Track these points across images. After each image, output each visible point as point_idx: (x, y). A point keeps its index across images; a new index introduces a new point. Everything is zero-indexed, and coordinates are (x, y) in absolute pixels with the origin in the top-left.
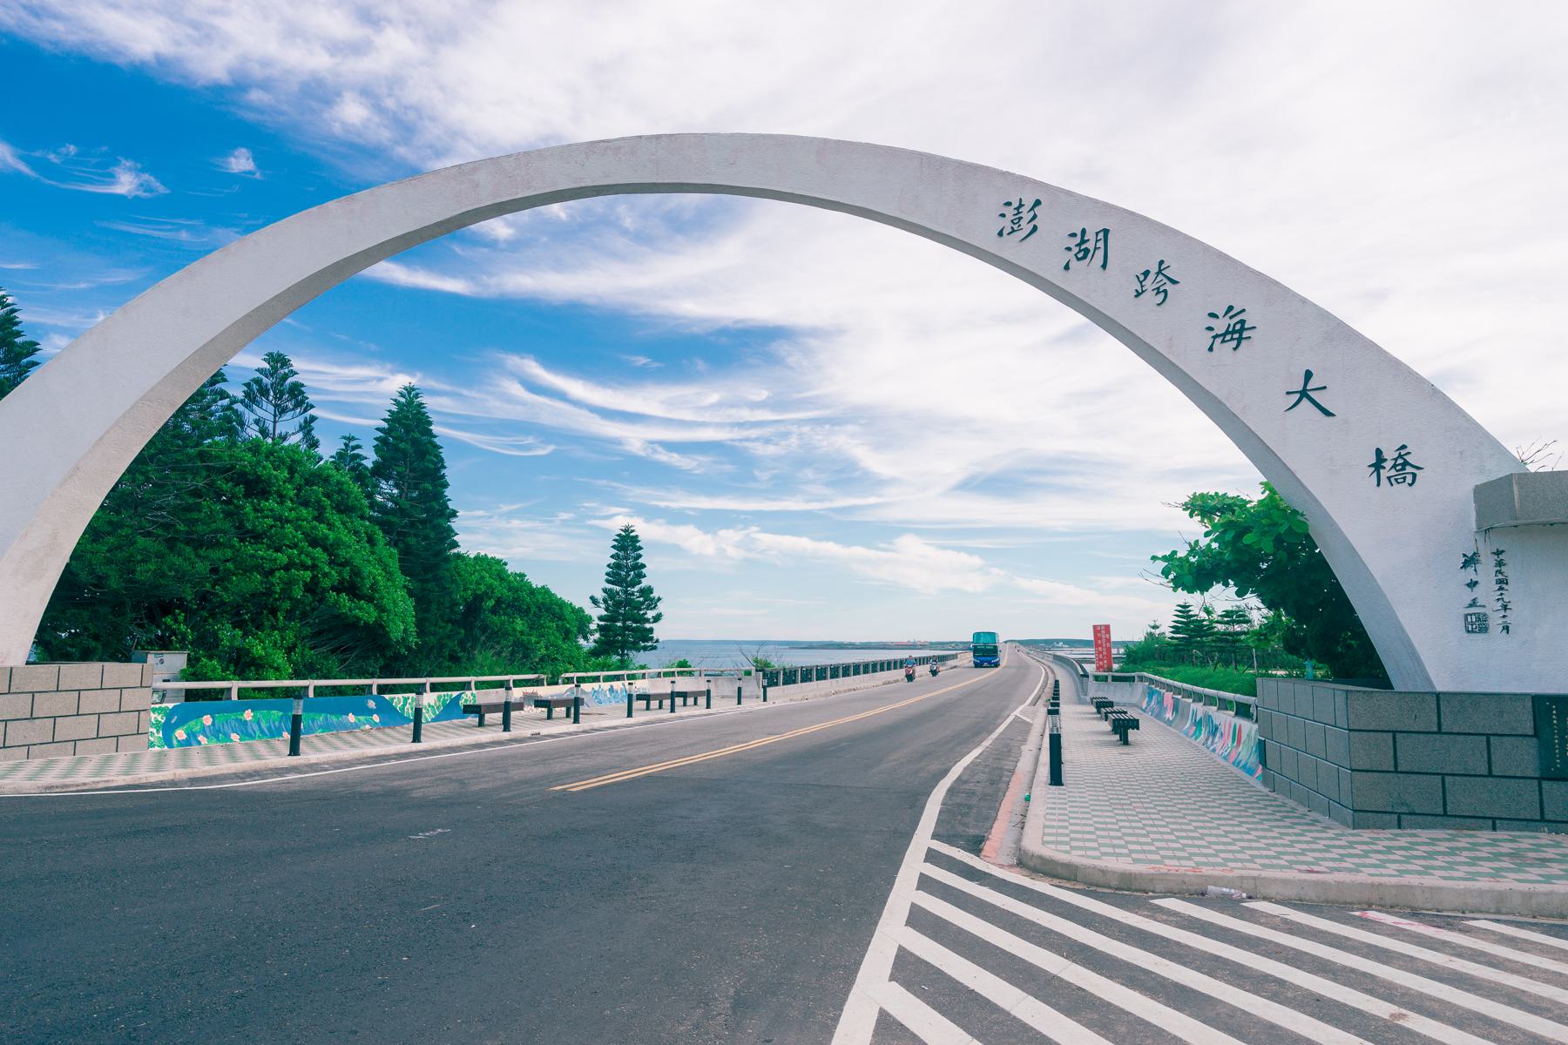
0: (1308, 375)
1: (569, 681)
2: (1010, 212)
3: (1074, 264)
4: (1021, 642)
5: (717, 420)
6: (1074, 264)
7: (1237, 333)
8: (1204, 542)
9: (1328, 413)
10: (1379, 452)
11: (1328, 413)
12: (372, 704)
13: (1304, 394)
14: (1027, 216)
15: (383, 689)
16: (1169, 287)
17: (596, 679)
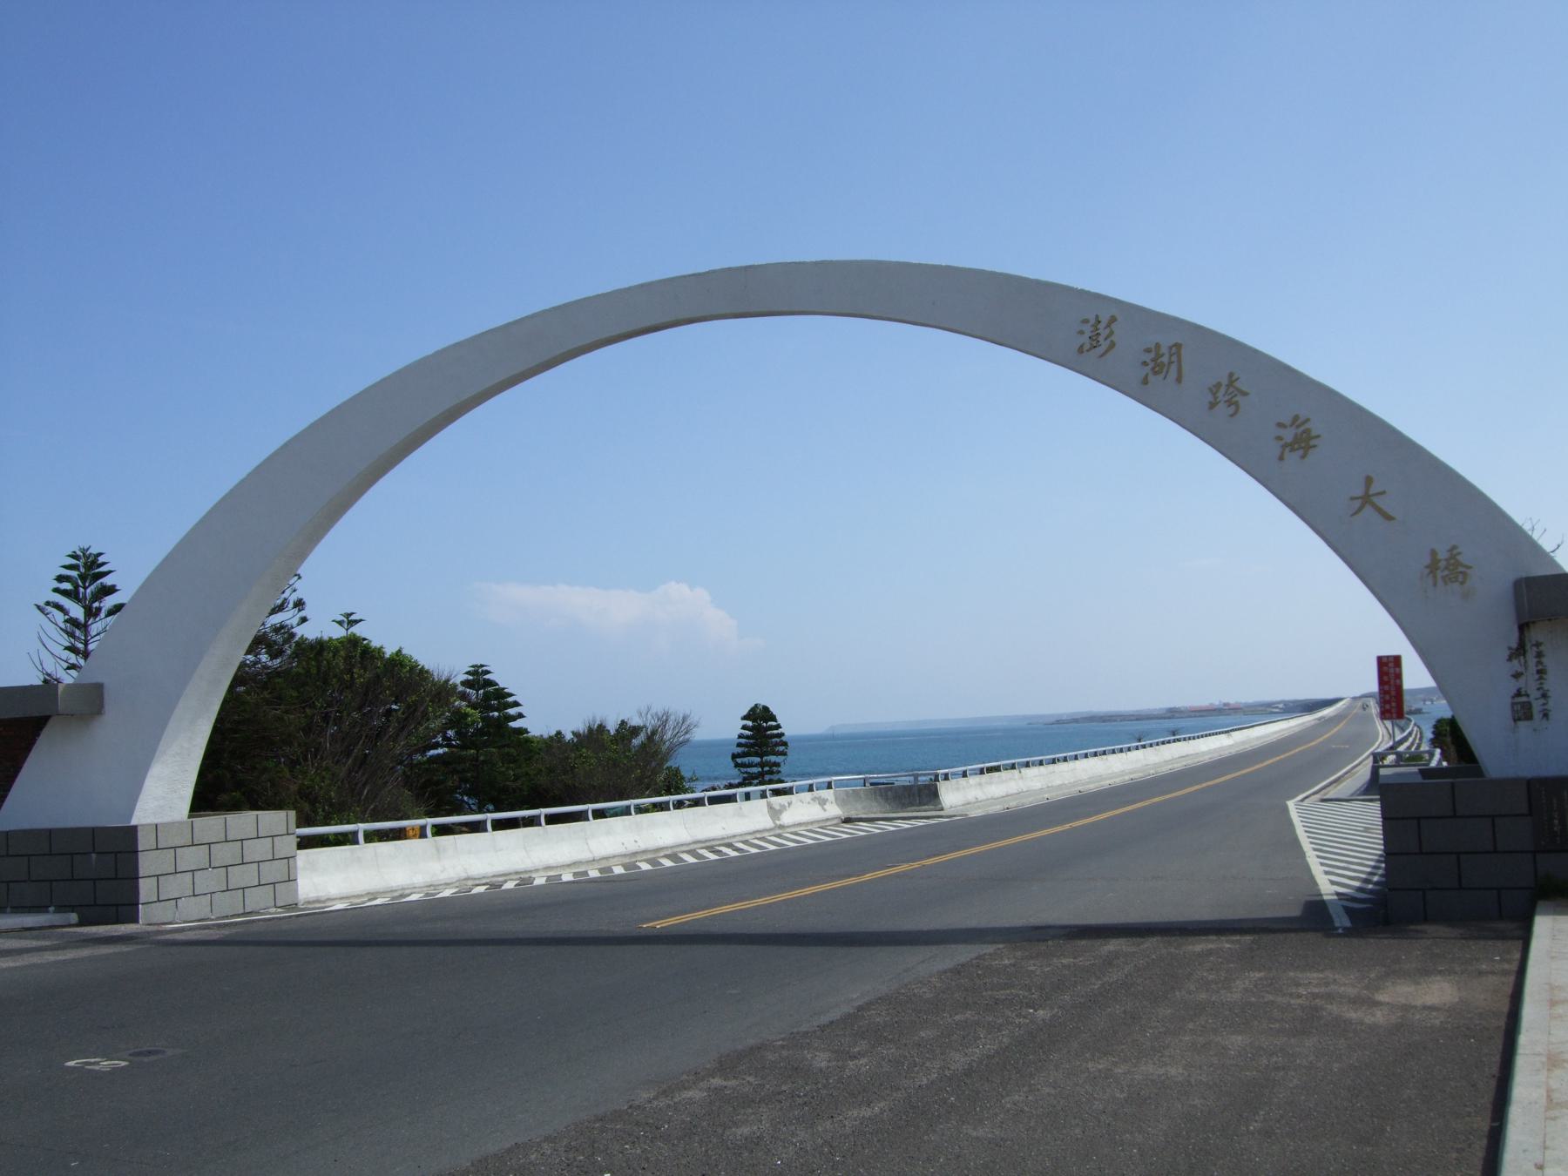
0: (1369, 481)
2: (1088, 329)
3: (1151, 378)
11: (1389, 518)
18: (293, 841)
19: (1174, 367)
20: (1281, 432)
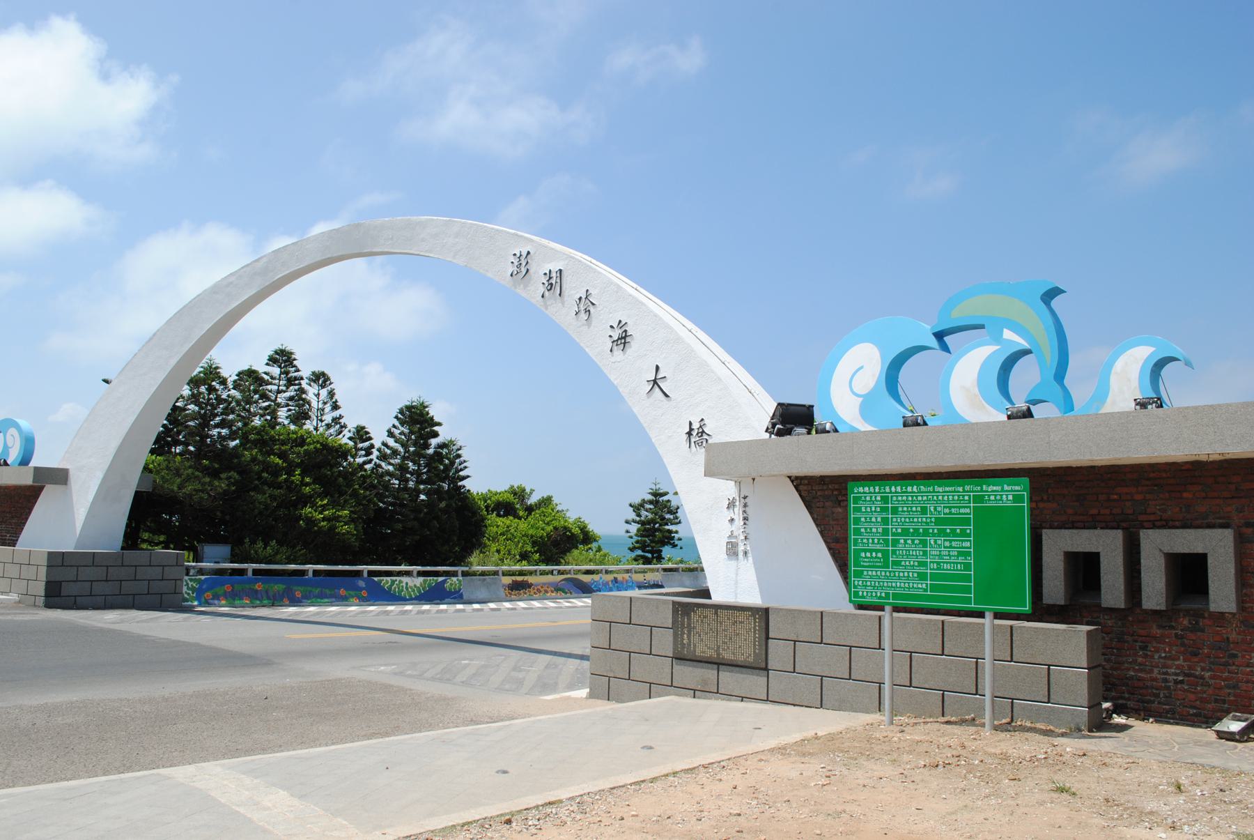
3: (547, 293)
4: (843, 568)
5: (1047, 574)
11: (666, 396)
13: (655, 382)
15: (371, 573)
17: (408, 573)
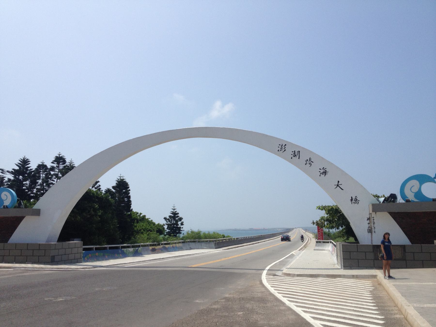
0: (338, 182)
1: (162, 244)
2: (280, 146)
3: (293, 157)
6: (293, 157)
7: (325, 173)
8: (326, 216)
9: (342, 189)
10: (352, 197)
11: (342, 189)
12: (120, 251)
13: (338, 185)
14: (283, 148)
16: (312, 163)
18: (82, 249)
19: (298, 156)
20: (320, 170)
